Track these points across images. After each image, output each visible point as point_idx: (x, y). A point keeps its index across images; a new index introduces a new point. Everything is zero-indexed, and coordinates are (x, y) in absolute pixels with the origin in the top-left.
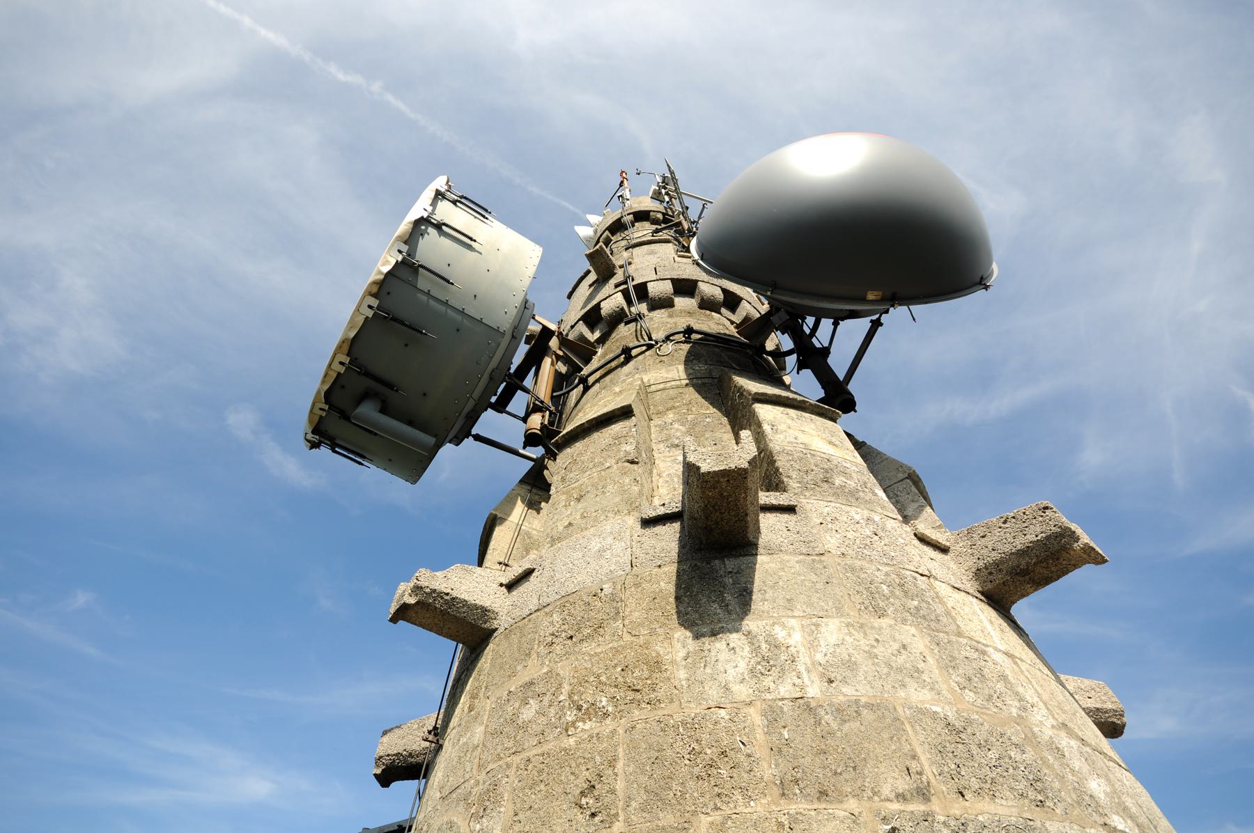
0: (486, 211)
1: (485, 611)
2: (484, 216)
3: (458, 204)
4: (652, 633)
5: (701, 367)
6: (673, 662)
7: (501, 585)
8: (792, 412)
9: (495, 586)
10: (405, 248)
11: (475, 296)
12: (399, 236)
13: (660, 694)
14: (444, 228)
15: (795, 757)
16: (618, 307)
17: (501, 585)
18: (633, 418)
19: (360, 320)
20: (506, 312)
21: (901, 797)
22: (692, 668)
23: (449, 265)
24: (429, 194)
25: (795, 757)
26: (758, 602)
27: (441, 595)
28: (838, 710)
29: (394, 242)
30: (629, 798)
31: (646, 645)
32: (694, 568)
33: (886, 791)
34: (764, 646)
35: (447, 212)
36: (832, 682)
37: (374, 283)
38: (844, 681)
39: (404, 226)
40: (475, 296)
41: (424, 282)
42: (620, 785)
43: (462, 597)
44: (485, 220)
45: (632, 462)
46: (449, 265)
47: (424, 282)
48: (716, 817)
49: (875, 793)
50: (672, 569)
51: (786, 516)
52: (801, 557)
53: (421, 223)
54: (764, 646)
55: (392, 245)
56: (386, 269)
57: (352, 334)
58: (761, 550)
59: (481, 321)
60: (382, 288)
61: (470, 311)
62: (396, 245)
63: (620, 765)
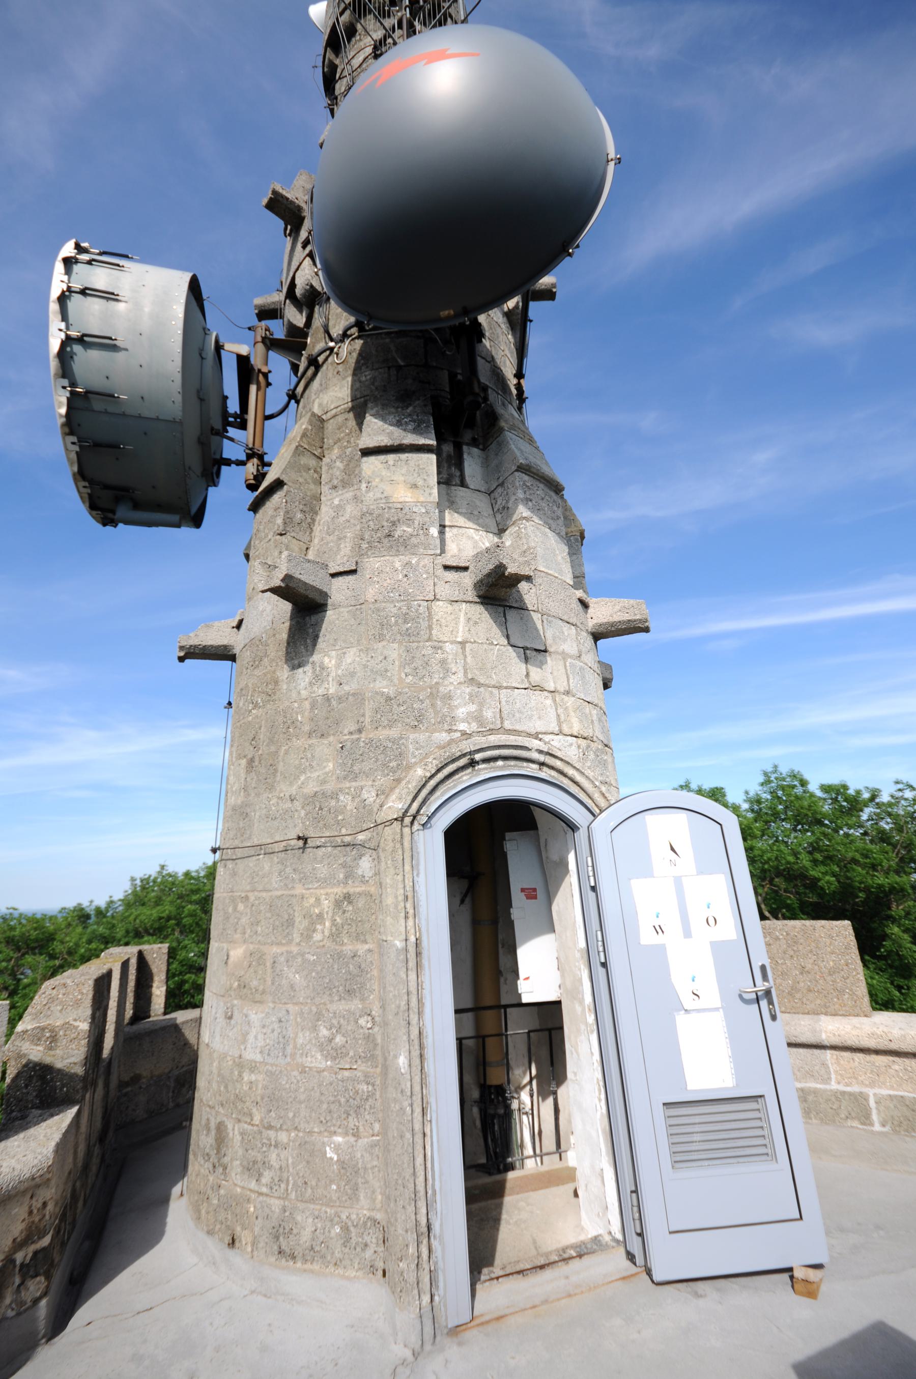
0: (113, 294)
1: (225, 647)
2: (118, 265)
3: (93, 263)
4: (277, 665)
5: (367, 375)
6: (283, 680)
7: (233, 627)
8: (391, 458)
9: (230, 629)
10: (65, 382)
11: (142, 398)
12: (56, 374)
13: (276, 697)
14: (86, 339)
15: (317, 722)
16: (307, 285)
17: (233, 627)
18: (285, 487)
19: (74, 456)
20: (173, 402)
21: (351, 733)
22: (288, 683)
23: (107, 378)
24: (59, 267)
25: (317, 722)
26: (321, 644)
27: (195, 646)
28: (339, 698)
29: (55, 381)
30: (264, 742)
31: (274, 672)
32: (298, 622)
33: (346, 732)
34: (318, 669)
35: (85, 276)
36: (341, 684)
37: (63, 425)
38: (347, 684)
39: (53, 364)
40: (142, 398)
41: (98, 405)
42: (261, 737)
43: (209, 644)
44: (122, 269)
45: (281, 535)
46: (107, 378)
47: (98, 405)
48: (287, 747)
49: (341, 733)
50: (287, 624)
51: (350, 577)
52: (351, 608)
53: (64, 355)
54: (318, 669)
55: (55, 386)
56: (63, 410)
57: (76, 469)
58: (329, 607)
59: (158, 419)
60: (71, 425)
61: (146, 413)
62: (57, 384)
63: (262, 728)
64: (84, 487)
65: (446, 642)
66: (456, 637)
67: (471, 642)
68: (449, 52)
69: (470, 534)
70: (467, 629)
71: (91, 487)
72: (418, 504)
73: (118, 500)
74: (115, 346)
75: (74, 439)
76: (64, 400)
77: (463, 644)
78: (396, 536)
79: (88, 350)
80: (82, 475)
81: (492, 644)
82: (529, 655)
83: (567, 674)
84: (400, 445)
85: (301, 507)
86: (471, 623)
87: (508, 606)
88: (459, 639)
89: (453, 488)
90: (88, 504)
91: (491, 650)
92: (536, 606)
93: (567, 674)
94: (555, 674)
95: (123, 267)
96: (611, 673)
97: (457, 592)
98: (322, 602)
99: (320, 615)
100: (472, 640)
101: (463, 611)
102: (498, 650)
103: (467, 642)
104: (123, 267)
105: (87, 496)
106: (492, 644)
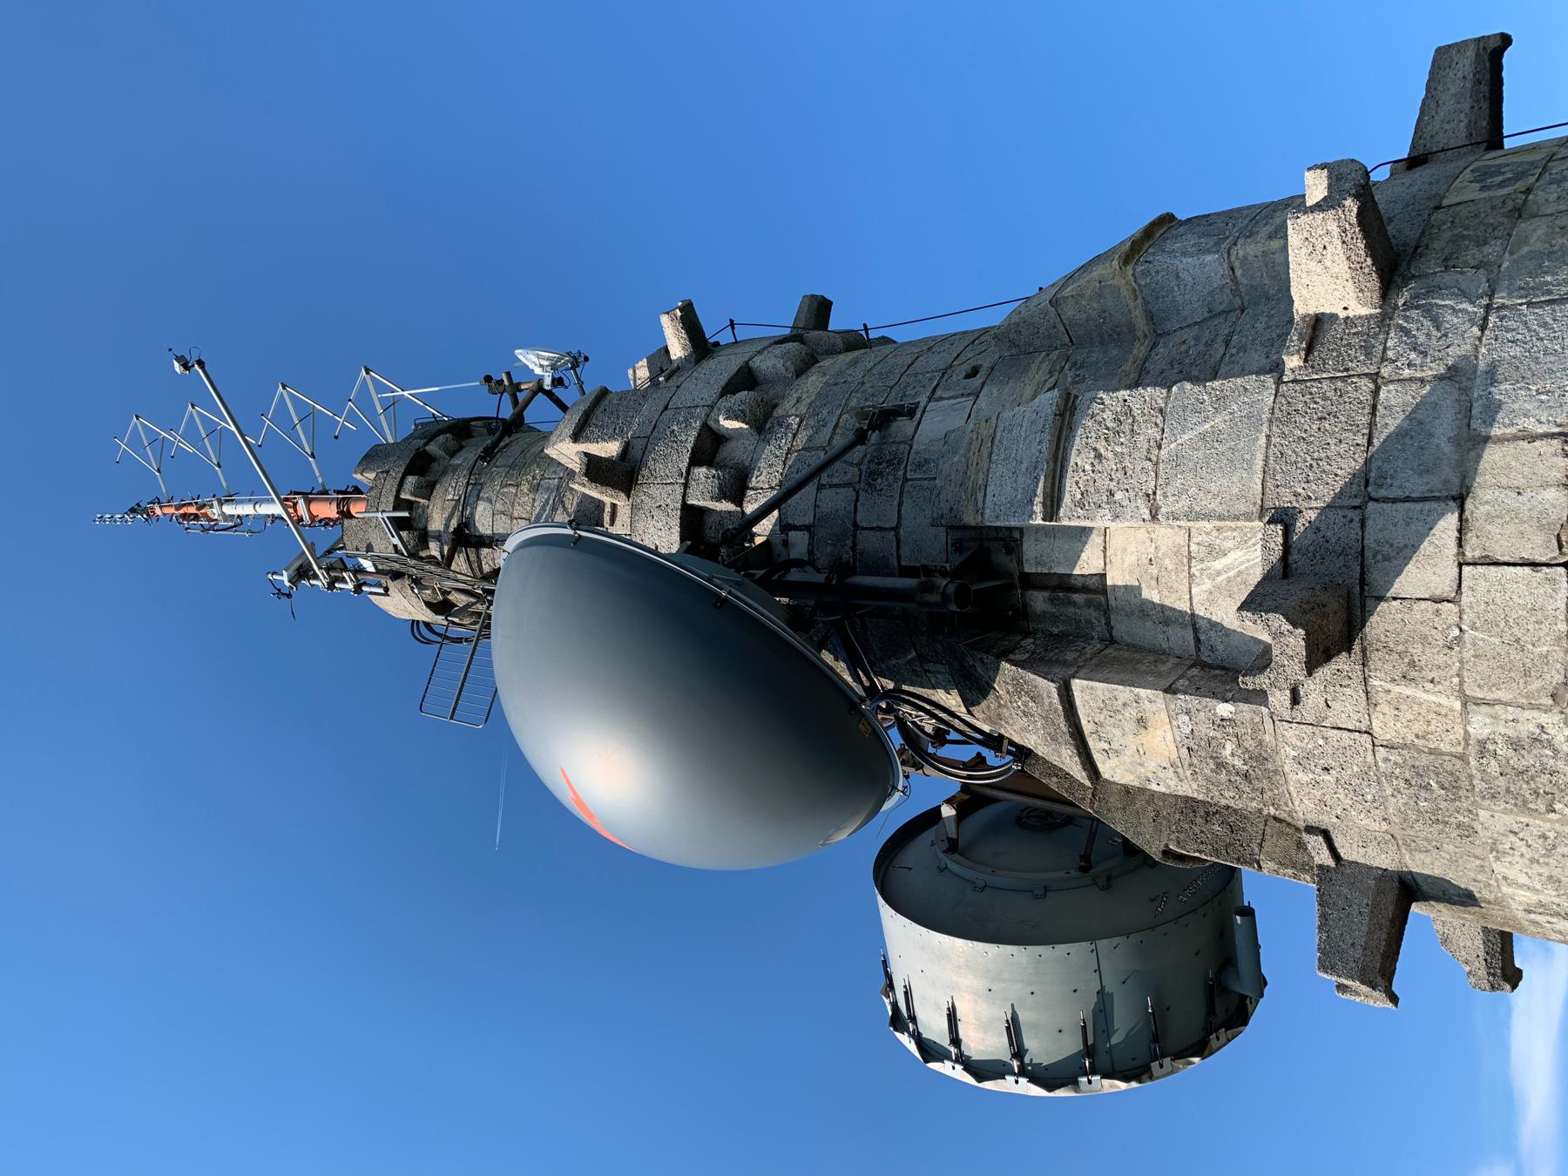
2: (906, 993)
19: (1179, 1063)
64: (1218, 1038)
65: (1466, 732)
66: (1452, 710)
67: (1461, 683)
68: (574, 797)
69: (1205, 596)
70: (1429, 686)
71: (1217, 1030)
72: (1175, 723)
73: (1225, 990)
74: (1012, 1019)
75: (1155, 1065)
76: (1106, 1082)
77: (1466, 701)
78: (1245, 767)
79: (1026, 1048)
80: (1202, 1048)
81: (1459, 640)
82: (1477, 554)
83: (1515, 438)
84: (1072, 735)
85: (1199, 820)
86: (1413, 674)
87: (1362, 590)
88: (1457, 705)
89: (1112, 602)
90: (1241, 1028)
91: (1474, 644)
92: (1350, 514)
93: (1515, 438)
94: (1520, 481)
95: (905, 986)
96: (1460, 47)
97: (1348, 691)
98: (1396, 884)
99: (1419, 880)
100: (1456, 680)
101: (1388, 686)
102: (1473, 627)
103: (1461, 691)
104: (905, 986)
105: (1229, 1032)
106: (1459, 640)
